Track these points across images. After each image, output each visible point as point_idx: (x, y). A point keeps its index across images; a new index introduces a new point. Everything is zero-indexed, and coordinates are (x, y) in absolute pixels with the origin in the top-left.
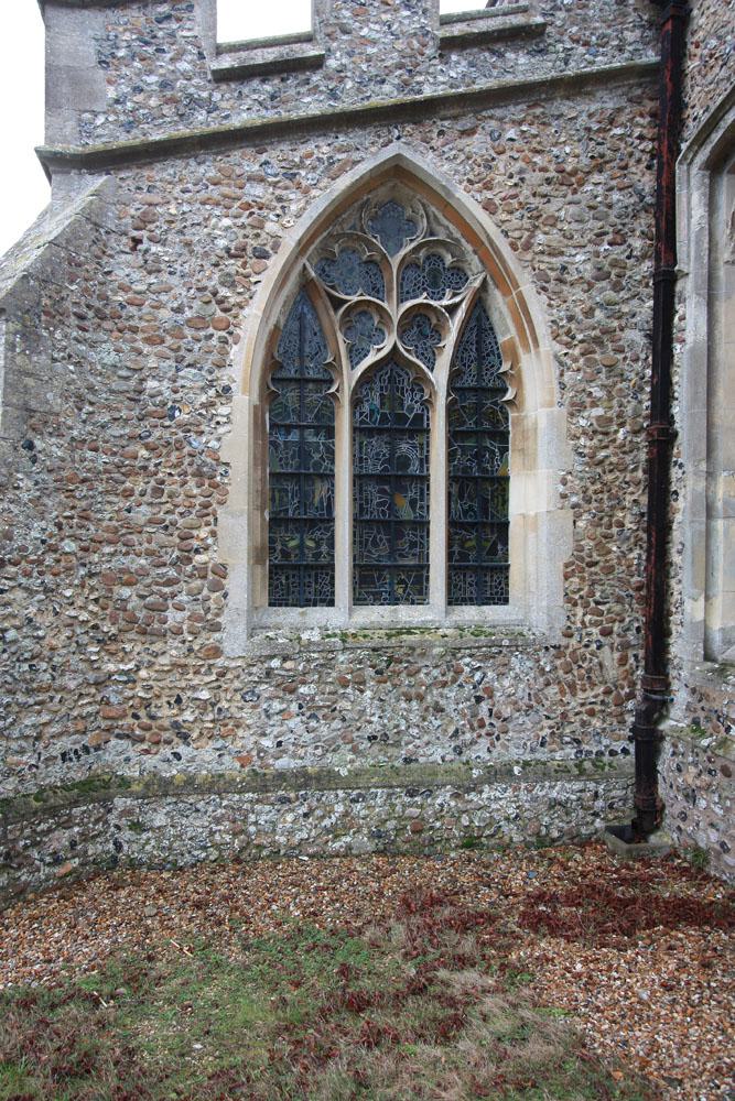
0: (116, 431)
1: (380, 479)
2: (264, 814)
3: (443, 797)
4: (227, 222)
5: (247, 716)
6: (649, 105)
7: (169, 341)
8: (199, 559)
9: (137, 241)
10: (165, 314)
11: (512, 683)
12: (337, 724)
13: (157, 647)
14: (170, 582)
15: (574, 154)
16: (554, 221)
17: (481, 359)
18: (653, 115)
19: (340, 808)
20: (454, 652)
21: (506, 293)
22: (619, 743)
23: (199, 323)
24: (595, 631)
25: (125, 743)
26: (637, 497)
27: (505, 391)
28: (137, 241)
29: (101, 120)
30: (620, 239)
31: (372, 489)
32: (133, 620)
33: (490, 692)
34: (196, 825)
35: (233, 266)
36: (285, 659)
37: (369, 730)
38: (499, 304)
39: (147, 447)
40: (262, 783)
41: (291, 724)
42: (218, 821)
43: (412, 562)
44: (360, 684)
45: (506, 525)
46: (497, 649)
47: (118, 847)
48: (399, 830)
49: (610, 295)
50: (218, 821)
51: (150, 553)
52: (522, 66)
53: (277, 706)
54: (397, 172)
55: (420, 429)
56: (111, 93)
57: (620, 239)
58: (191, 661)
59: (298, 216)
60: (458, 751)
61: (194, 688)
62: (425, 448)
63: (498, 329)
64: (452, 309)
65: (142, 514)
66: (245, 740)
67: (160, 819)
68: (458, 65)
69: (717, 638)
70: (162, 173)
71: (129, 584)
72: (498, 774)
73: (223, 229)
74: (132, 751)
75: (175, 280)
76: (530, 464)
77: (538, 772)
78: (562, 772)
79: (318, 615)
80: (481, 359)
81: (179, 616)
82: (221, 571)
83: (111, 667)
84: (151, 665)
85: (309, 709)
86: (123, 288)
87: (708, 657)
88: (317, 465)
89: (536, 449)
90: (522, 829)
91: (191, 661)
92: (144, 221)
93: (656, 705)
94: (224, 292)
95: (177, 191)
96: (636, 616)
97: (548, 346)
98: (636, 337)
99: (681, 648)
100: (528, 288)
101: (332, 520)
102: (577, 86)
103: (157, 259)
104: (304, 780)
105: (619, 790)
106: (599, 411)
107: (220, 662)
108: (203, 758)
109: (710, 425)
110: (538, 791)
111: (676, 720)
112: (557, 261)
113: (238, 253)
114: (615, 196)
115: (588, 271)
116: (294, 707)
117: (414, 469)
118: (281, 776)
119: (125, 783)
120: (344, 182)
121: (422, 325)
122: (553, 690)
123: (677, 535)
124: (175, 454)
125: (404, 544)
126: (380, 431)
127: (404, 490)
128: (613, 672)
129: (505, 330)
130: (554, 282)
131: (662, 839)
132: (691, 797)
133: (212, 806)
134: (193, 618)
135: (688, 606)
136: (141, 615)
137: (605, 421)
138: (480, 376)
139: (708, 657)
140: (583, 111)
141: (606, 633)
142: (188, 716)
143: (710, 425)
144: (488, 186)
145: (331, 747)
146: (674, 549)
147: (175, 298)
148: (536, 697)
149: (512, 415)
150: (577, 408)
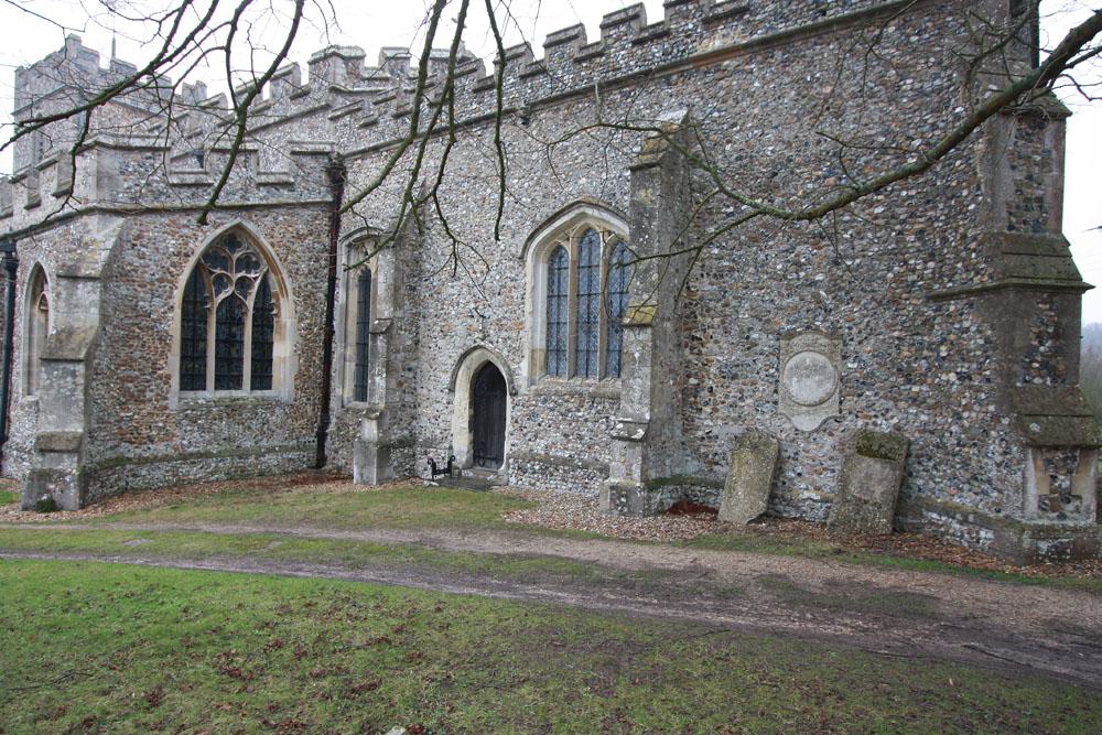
0: (126, 321)
1: (225, 341)
2: (184, 469)
3: (252, 459)
4: (173, 242)
5: (177, 432)
6: (329, 214)
7: (149, 287)
8: (160, 372)
9: (134, 245)
10: (147, 276)
11: (276, 417)
12: (212, 434)
13: (142, 406)
14: (148, 381)
15: (302, 229)
16: (295, 251)
17: (264, 298)
18: (330, 218)
19: (213, 465)
20: (256, 407)
21: (276, 274)
22: (312, 439)
23: (161, 280)
24: (304, 399)
25: (127, 444)
26: (320, 352)
27: (272, 310)
28: (134, 245)
29: (120, 195)
30: (317, 261)
31: (222, 345)
32: (132, 396)
33: (268, 421)
34: (158, 474)
35: (175, 259)
36: (193, 410)
37: (223, 436)
38: (273, 278)
39: (140, 328)
40: (185, 457)
41: (195, 434)
42: (167, 472)
43: (236, 373)
44: (221, 419)
45: (272, 360)
46: (270, 405)
47: (127, 483)
48: (235, 471)
49: (313, 279)
50: (167, 472)
51: (139, 370)
52: (285, 196)
53: (189, 428)
54: (239, 227)
55: (241, 323)
56: (126, 185)
57: (317, 261)
58: (156, 412)
59: (202, 241)
60: (256, 443)
61: (156, 422)
62: (242, 330)
63: (271, 287)
64: (255, 279)
65: (137, 354)
66: (177, 441)
67: (144, 472)
68: (263, 192)
69: (346, 401)
70: (146, 219)
71: (131, 382)
72: (271, 450)
73: (172, 244)
74: (131, 447)
75: (150, 263)
76: (283, 338)
77: (285, 449)
78: (293, 449)
79: (200, 394)
80: (264, 298)
81: (152, 394)
82: (168, 377)
83: (123, 414)
84: (139, 413)
85: (202, 429)
86: (130, 264)
87: (343, 407)
88: (201, 335)
89: (784, 553)
90: (279, 469)
91: (156, 412)
92: (139, 237)
93: (325, 423)
94: (172, 269)
95: (152, 227)
96: (319, 394)
97: (291, 297)
98: (321, 295)
99: (334, 404)
100: (285, 275)
101: (206, 357)
102: (305, 205)
103: (144, 253)
104: (200, 455)
105: (312, 454)
106: (308, 321)
107: (167, 412)
108: (160, 448)
109: (346, 331)
110: (284, 456)
111: (332, 428)
112: (296, 266)
113: (178, 254)
114: (316, 245)
115: (306, 271)
116: (196, 428)
117: (238, 338)
118: (191, 454)
119: (129, 459)
120: (219, 231)
121: (244, 284)
122: (290, 420)
123: (333, 366)
124: (150, 332)
125: (233, 367)
126: (225, 323)
127: (233, 346)
128: (310, 413)
129: (274, 288)
130: (294, 274)
131: (328, 467)
132: (336, 452)
133: (165, 466)
134: (158, 395)
135: (337, 390)
136: (136, 393)
137: (310, 325)
138: (264, 304)
139: (343, 407)
140: (306, 213)
141: (309, 400)
142: (154, 433)
143: (346, 331)
144: (272, 237)
145: (209, 443)
146: (332, 371)
147: (152, 271)
148: (284, 423)
149: (275, 319)
150: (301, 320)
